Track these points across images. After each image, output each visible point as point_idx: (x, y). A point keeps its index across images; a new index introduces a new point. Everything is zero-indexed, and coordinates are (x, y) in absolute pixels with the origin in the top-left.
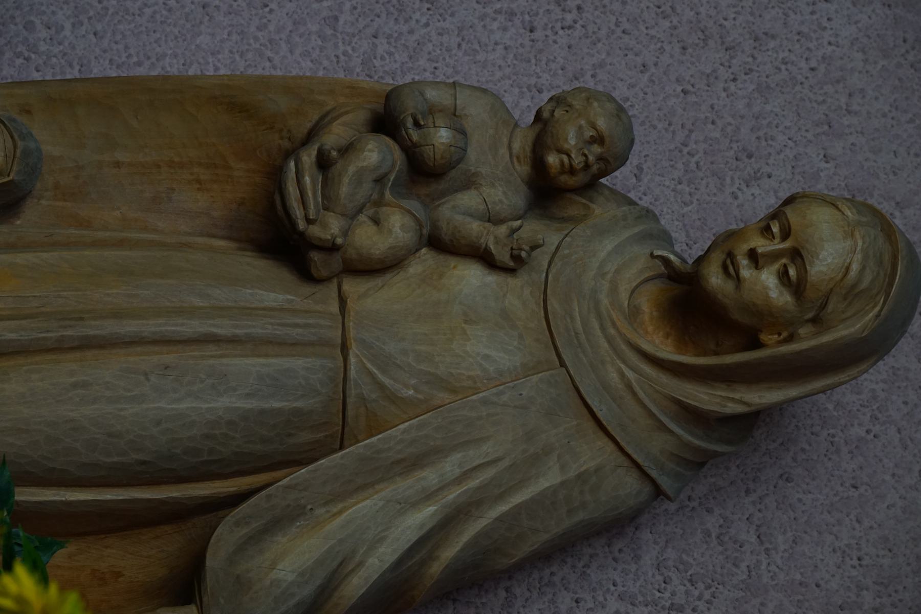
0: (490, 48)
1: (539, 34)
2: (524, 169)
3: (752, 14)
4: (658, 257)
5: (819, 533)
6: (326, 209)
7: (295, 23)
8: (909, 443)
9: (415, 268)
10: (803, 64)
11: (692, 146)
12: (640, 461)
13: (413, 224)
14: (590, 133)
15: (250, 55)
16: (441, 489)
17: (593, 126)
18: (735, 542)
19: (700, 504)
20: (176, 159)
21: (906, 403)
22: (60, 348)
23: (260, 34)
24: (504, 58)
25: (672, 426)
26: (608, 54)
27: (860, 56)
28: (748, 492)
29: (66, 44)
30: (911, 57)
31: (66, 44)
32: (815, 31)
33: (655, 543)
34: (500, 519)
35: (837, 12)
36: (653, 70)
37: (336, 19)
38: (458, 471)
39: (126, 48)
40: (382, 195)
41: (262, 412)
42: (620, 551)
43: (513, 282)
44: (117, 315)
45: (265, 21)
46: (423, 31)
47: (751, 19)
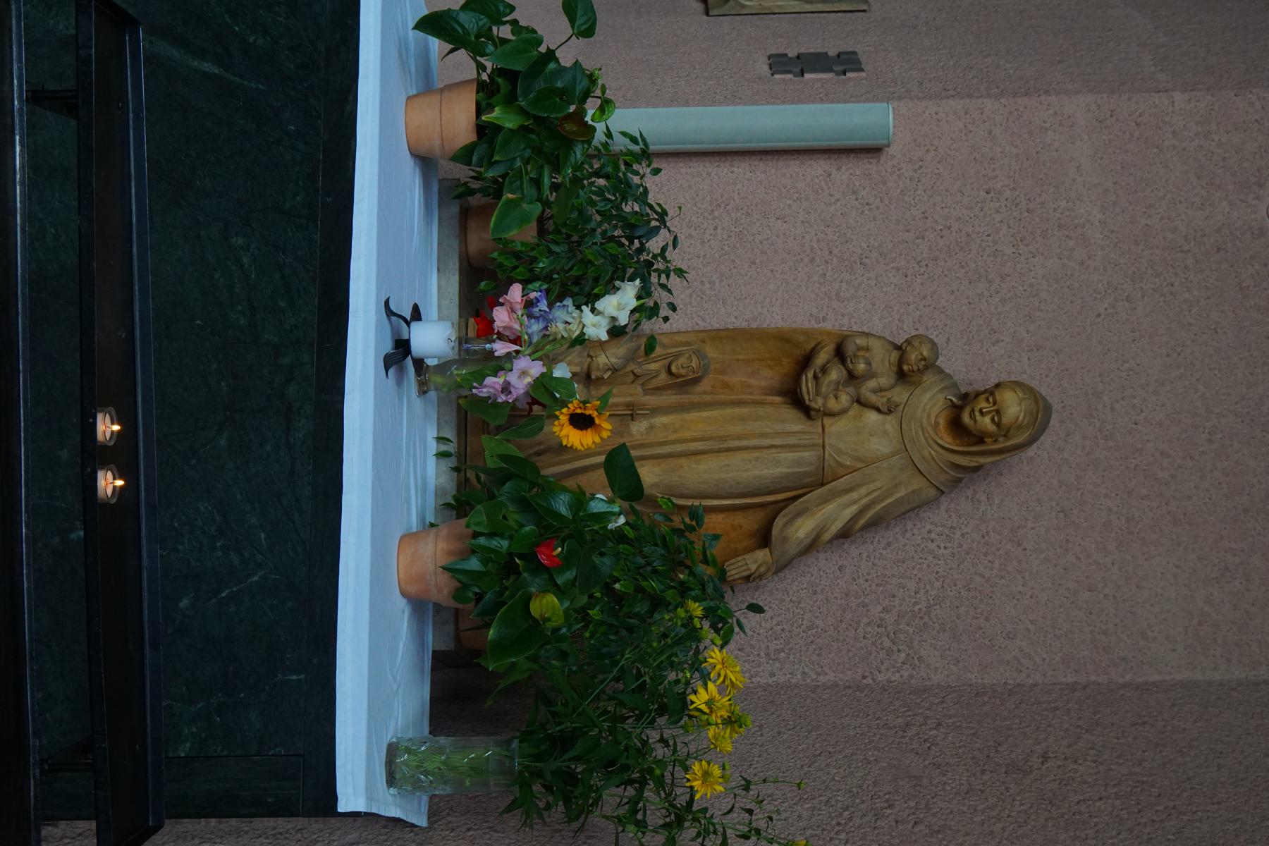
1: (909, 278)
2: (895, 369)
7: (808, 277)
9: (851, 413)
10: (1021, 288)
14: (920, 357)
17: (922, 355)
22: (719, 451)
28: (984, 480)
34: (882, 509)
36: (956, 293)
37: (825, 274)
39: (741, 291)
41: (793, 473)
43: (889, 418)
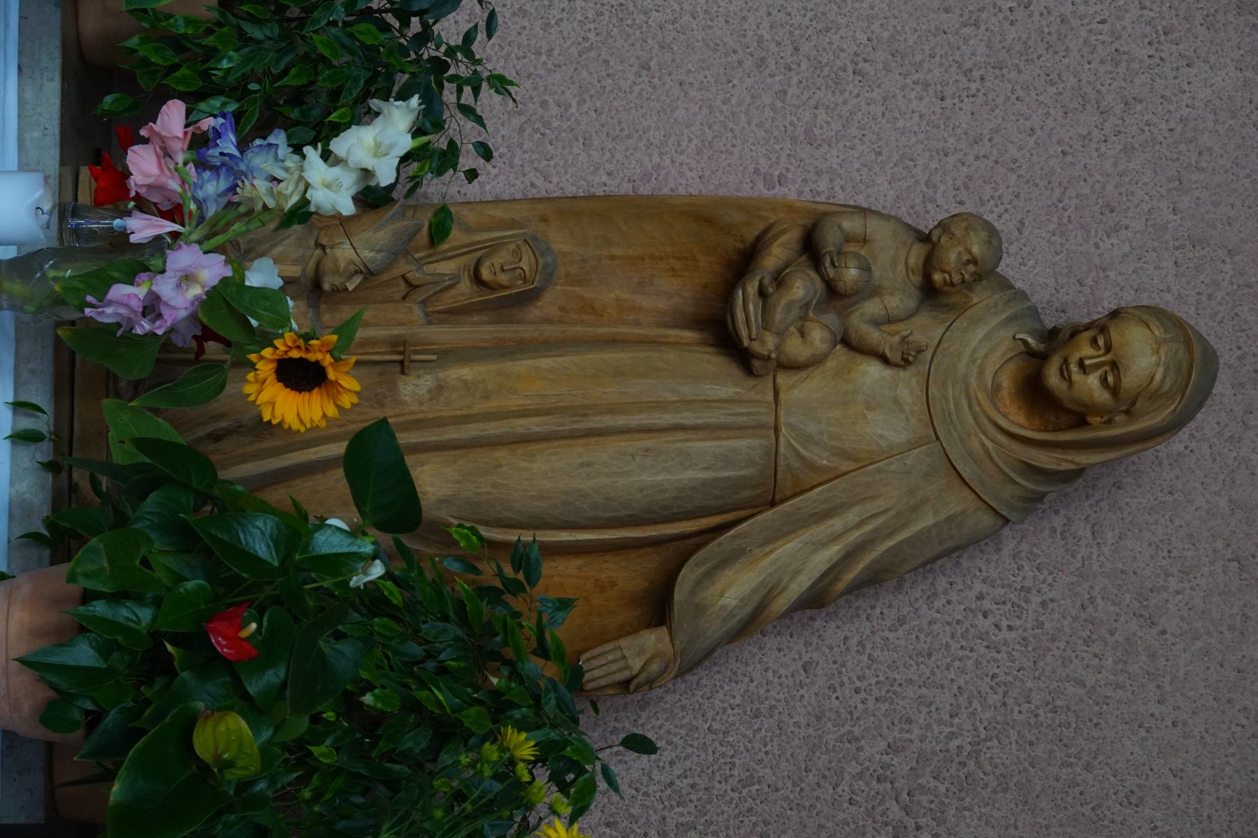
0: (908, 116)
1: (948, 102)
2: (917, 279)
3: (1125, 80)
4: (1020, 339)
5: (1140, 531)
6: (764, 329)
8: (1218, 457)
9: (831, 364)
10: (1164, 126)
11: (1066, 201)
12: (994, 505)
13: (829, 336)
14: (965, 257)
15: (716, 127)
16: (845, 532)
17: (970, 252)
18: (1074, 538)
19: (1050, 507)
20: (657, 254)
21: (1218, 423)
22: (572, 436)
23: (724, 108)
24: (919, 125)
25: (1019, 480)
26: (1003, 119)
27: (1211, 116)
28: (1087, 497)
29: (573, 120)
30: (1254, 117)
31: (573, 120)
32: (1176, 95)
33: (1014, 538)
35: (1196, 76)
36: (1039, 133)
37: (785, 92)
38: (858, 520)
39: (620, 122)
40: (807, 313)
41: (717, 479)
42: (986, 544)
44: (612, 410)
45: (729, 95)
46: (855, 101)
47: (1124, 84)
